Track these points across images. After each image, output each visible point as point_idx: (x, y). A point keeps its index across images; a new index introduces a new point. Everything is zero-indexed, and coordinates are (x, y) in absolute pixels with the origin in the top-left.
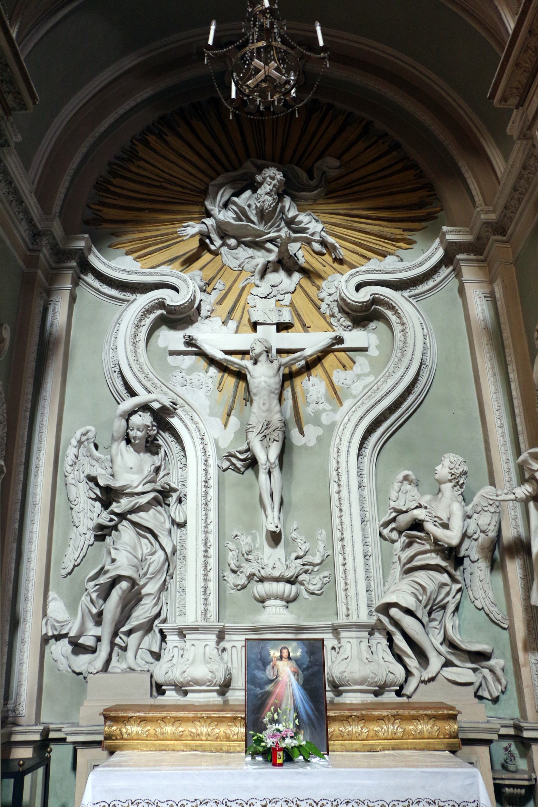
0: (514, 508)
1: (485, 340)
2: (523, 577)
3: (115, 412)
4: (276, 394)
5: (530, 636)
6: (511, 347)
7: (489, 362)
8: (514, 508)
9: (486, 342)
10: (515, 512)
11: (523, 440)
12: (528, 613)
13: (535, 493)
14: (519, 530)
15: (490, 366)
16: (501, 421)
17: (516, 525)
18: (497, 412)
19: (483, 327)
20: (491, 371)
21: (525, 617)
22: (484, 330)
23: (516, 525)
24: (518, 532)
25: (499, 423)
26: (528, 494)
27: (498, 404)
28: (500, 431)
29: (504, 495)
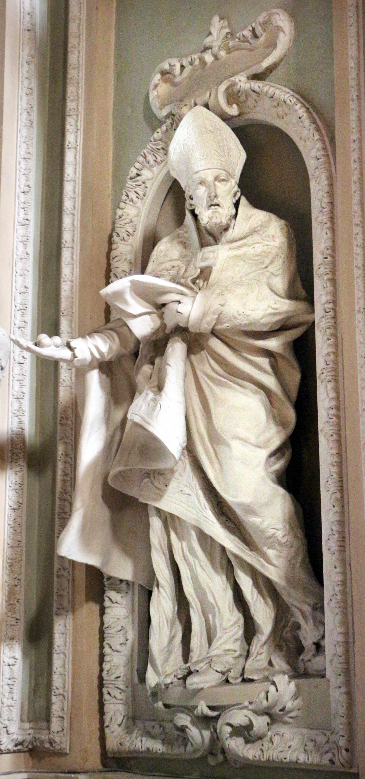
0: (20, 377)
1: (26, 52)
2: (15, 507)
3: (203, 41)
4: (72, 64)
5: (10, 614)
6: (82, 84)
7: (25, 98)
8: (20, 377)
9: (26, 58)
10: (21, 387)
11: (69, 259)
12: (12, 572)
13: (109, 357)
14: (23, 419)
15: (25, 105)
16: (26, 214)
17: (20, 409)
18: (22, 196)
19: (27, 25)
20: (25, 115)
21: (6, 578)
22: (27, 33)
23: (20, 409)
24: (20, 422)
25: (22, 216)
26: (97, 356)
27: (27, 180)
28: (21, 231)
29: (53, 347)
